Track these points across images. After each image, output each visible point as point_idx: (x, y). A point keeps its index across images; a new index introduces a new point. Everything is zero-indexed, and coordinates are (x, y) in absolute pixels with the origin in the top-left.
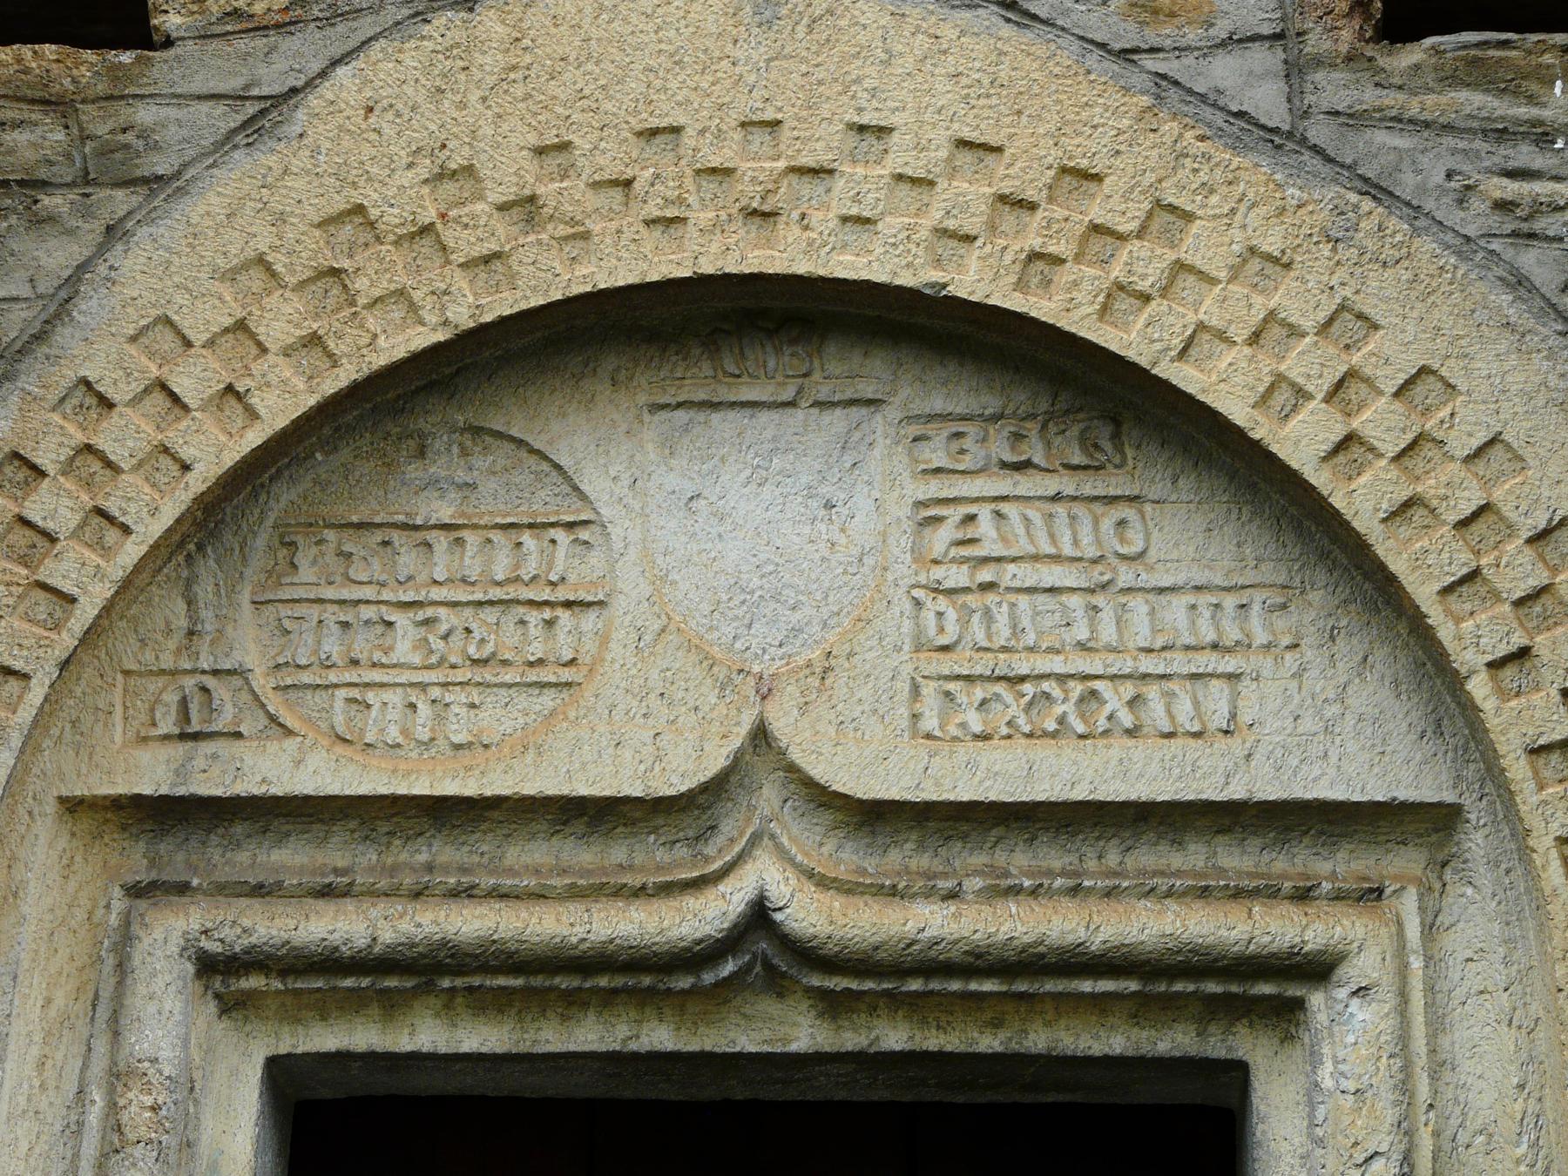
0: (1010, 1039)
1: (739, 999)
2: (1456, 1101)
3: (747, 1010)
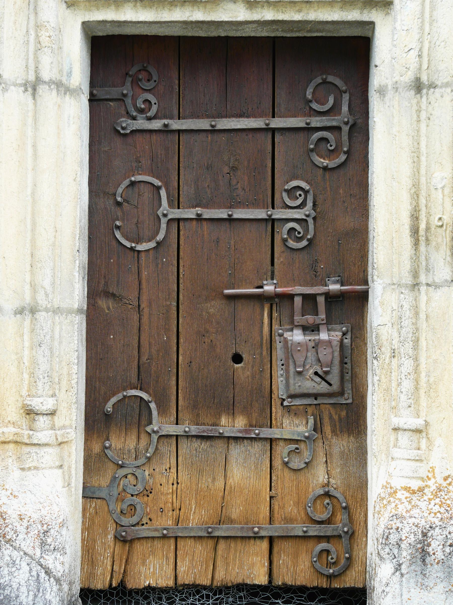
0: (304, 16)
1: (222, 4)
2: (437, 32)
3: (225, 7)
